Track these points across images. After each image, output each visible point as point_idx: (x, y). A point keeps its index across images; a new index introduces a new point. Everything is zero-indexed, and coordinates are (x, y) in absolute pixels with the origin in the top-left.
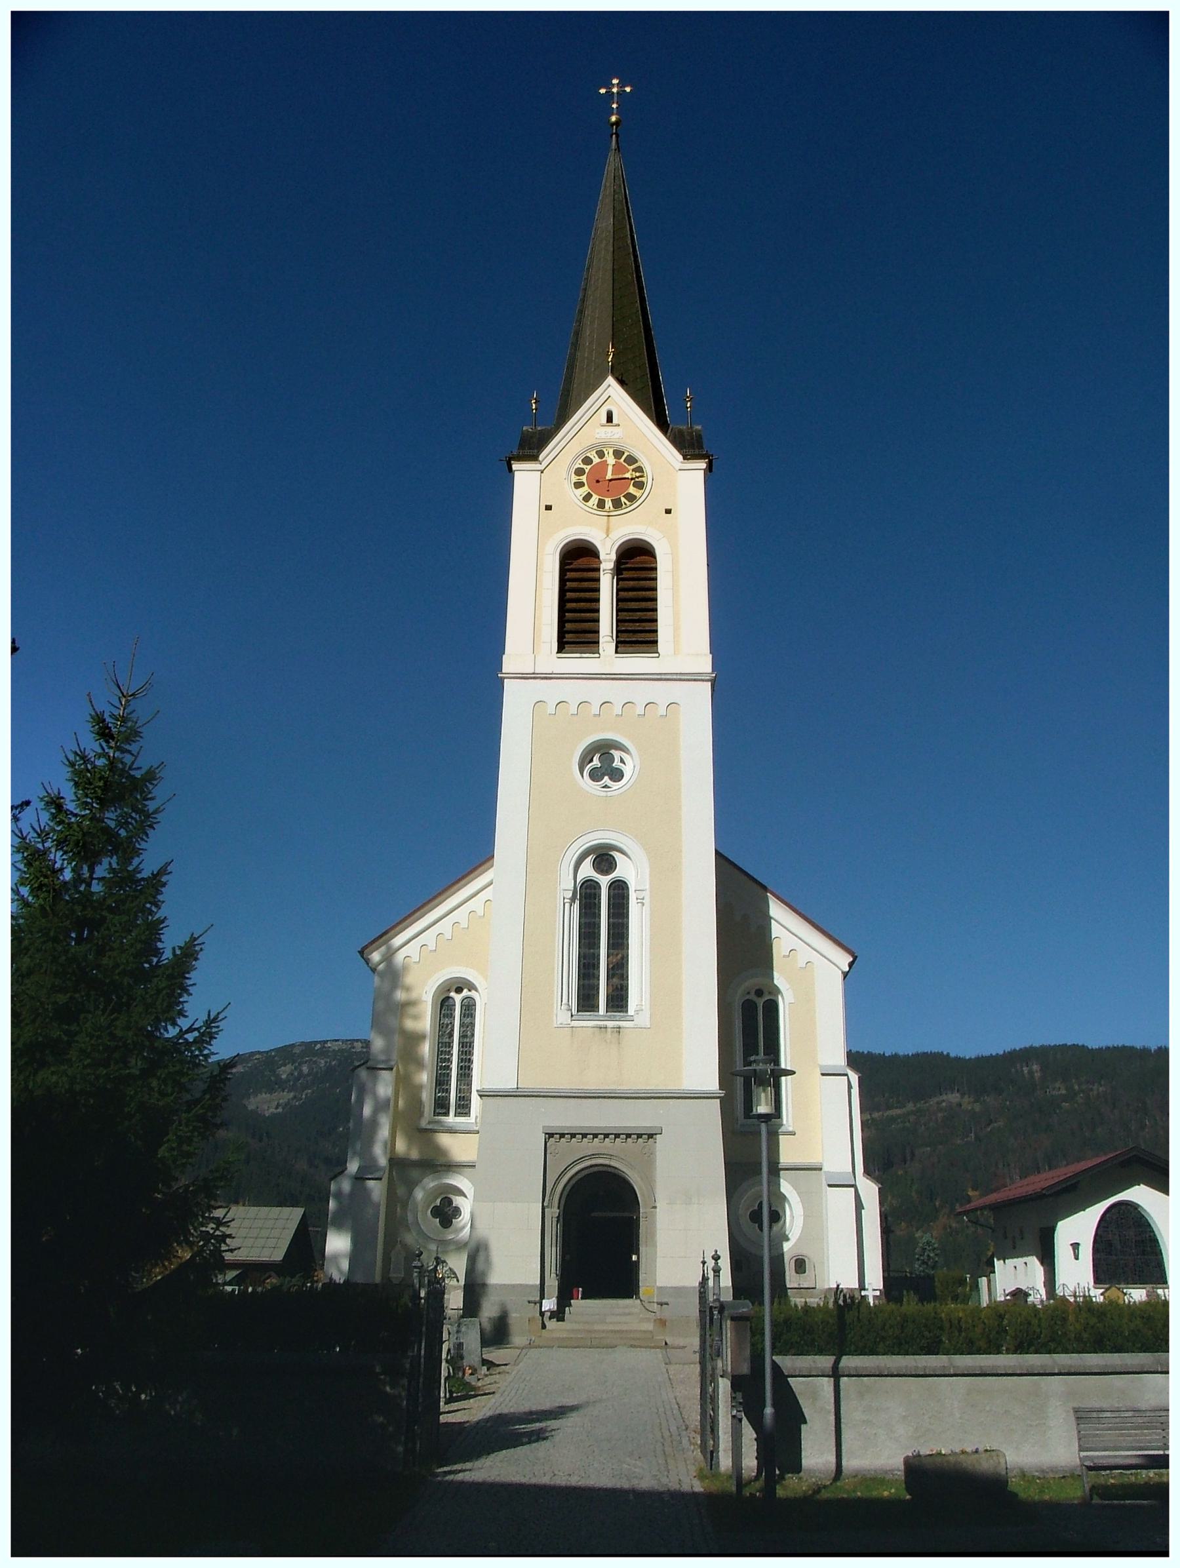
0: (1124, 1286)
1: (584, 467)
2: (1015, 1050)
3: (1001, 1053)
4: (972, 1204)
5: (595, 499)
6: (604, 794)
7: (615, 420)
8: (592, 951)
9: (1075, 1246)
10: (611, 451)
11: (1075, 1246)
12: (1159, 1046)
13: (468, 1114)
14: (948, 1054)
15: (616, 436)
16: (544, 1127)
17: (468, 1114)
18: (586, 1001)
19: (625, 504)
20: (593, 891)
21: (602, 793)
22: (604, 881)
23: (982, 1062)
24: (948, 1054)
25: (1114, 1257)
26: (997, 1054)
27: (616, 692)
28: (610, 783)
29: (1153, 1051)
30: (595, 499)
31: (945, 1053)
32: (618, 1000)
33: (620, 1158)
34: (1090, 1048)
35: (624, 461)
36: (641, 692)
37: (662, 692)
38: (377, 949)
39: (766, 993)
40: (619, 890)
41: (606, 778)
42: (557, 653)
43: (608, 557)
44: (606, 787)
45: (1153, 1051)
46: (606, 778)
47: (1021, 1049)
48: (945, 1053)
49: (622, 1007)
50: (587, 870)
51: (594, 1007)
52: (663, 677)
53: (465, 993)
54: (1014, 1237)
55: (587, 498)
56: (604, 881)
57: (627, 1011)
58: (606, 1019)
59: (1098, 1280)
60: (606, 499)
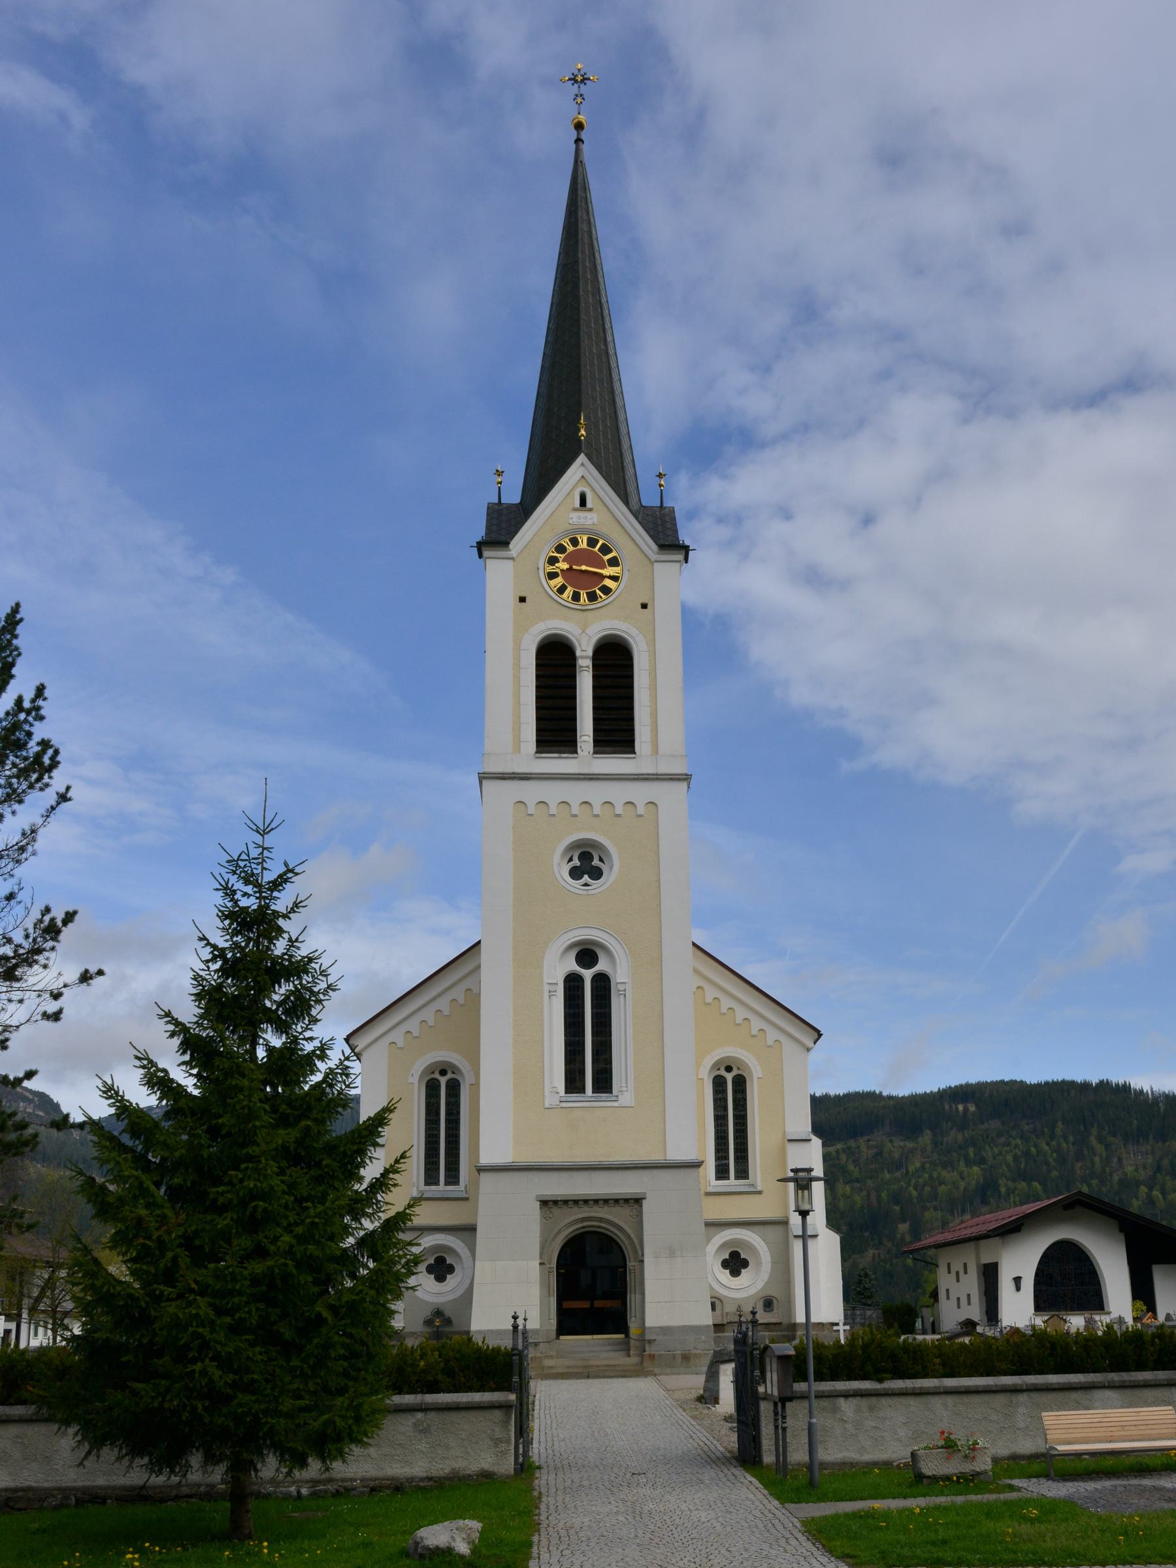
0: (1063, 1313)
1: (558, 555)
2: (950, 1087)
3: (936, 1090)
4: (921, 1243)
5: (569, 591)
6: (585, 893)
7: (589, 504)
8: (577, 1039)
9: (1017, 1281)
10: (585, 538)
11: (1017, 1281)
12: (1101, 1079)
13: (457, 1183)
14: (881, 1093)
15: (590, 522)
16: (537, 1196)
17: (457, 1183)
18: (574, 1083)
19: (601, 597)
20: (576, 984)
21: (582, 891)
22: (588, 974)
23: (916, 1101)
24: (881, 1093)
25: (1054, 1288)
26: (932, 1092)
27: (596, 793)
28: (590, 881)
29: (1094, 1085)
30: (569, 591)
31: (877, 1092)
32: (603, 1083)
33: (618, 1217)
34: (1028, 1083)
35: (599, 550)
36: (619, 793)
37: (640, 793)
38: (1042, 1315)
39: (735, 1068)
40: (602, 983)
41: (586, 876)
42: (536, 753)
43: (584, 654)
44: (586, 885)
45: (1094, 1085)
46: (586, 876)
47: (956, 1086)
48: (877, 1092)
49: (607, 1088)
50: (571, 965)
51: (582, 1090)
52: (640, 777)
53: (449, 1076)
54: (957, 1273)
55: (562, 590)
56: (588, 974)
57: (611, 1092)
58: (593, 1099)
59: (1039, 1307)
60: (582, 592)
